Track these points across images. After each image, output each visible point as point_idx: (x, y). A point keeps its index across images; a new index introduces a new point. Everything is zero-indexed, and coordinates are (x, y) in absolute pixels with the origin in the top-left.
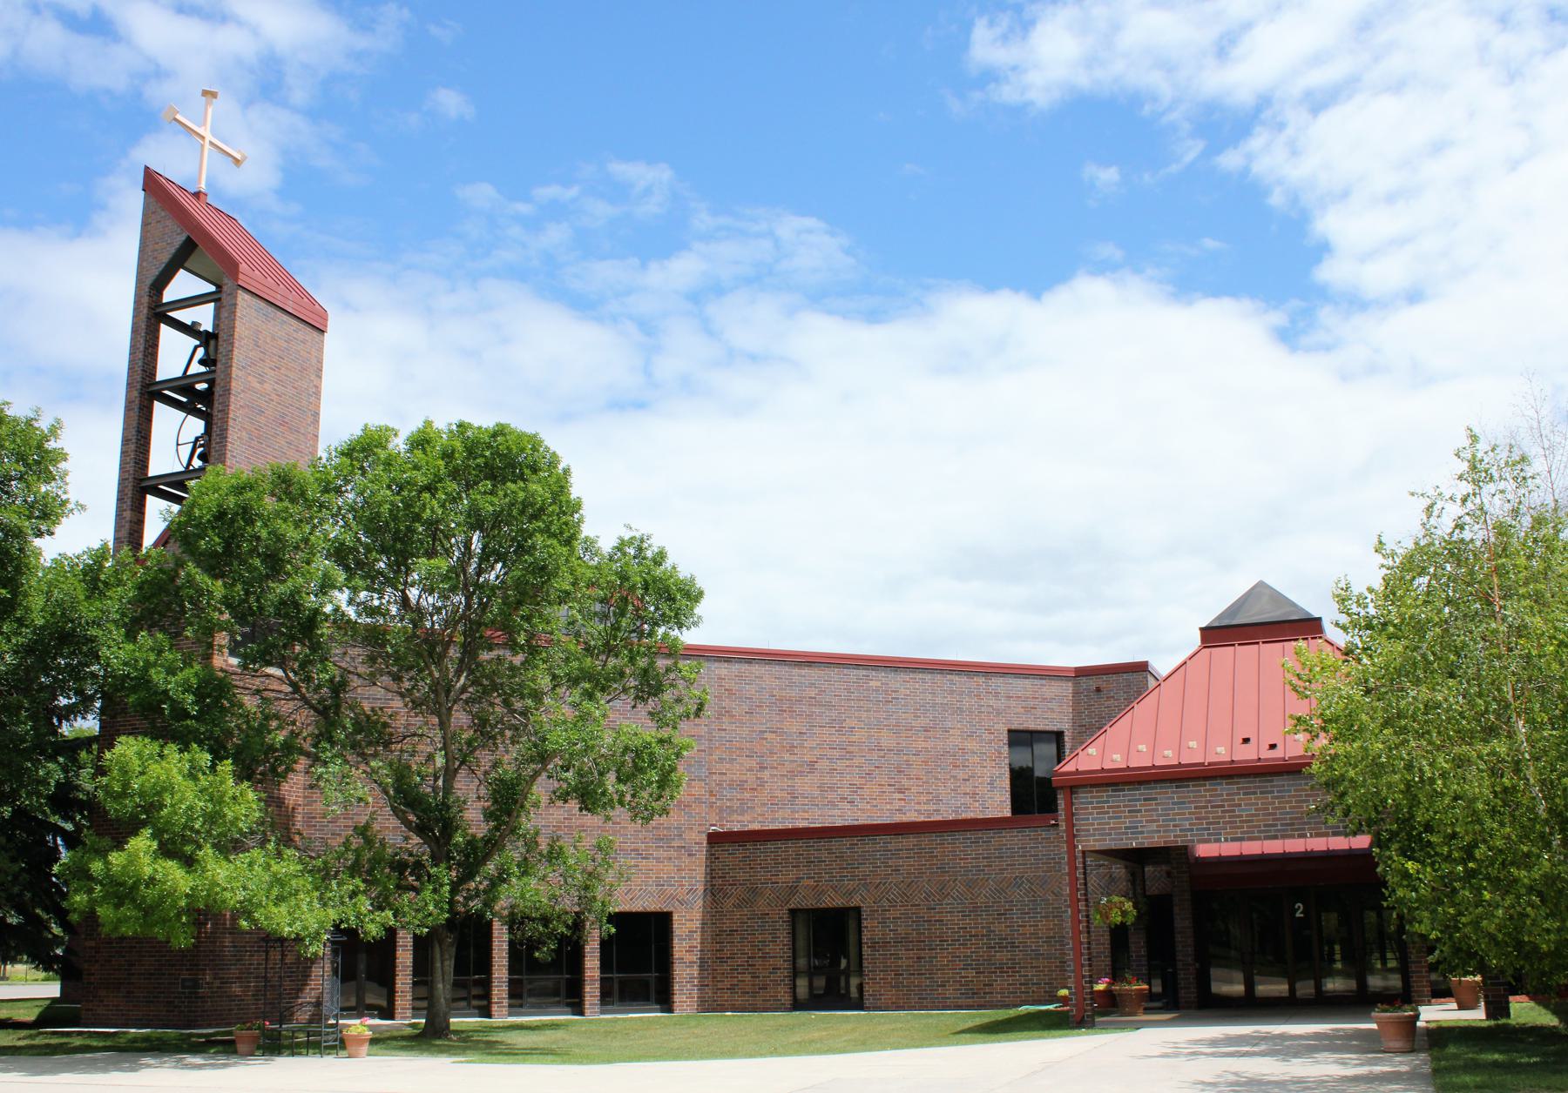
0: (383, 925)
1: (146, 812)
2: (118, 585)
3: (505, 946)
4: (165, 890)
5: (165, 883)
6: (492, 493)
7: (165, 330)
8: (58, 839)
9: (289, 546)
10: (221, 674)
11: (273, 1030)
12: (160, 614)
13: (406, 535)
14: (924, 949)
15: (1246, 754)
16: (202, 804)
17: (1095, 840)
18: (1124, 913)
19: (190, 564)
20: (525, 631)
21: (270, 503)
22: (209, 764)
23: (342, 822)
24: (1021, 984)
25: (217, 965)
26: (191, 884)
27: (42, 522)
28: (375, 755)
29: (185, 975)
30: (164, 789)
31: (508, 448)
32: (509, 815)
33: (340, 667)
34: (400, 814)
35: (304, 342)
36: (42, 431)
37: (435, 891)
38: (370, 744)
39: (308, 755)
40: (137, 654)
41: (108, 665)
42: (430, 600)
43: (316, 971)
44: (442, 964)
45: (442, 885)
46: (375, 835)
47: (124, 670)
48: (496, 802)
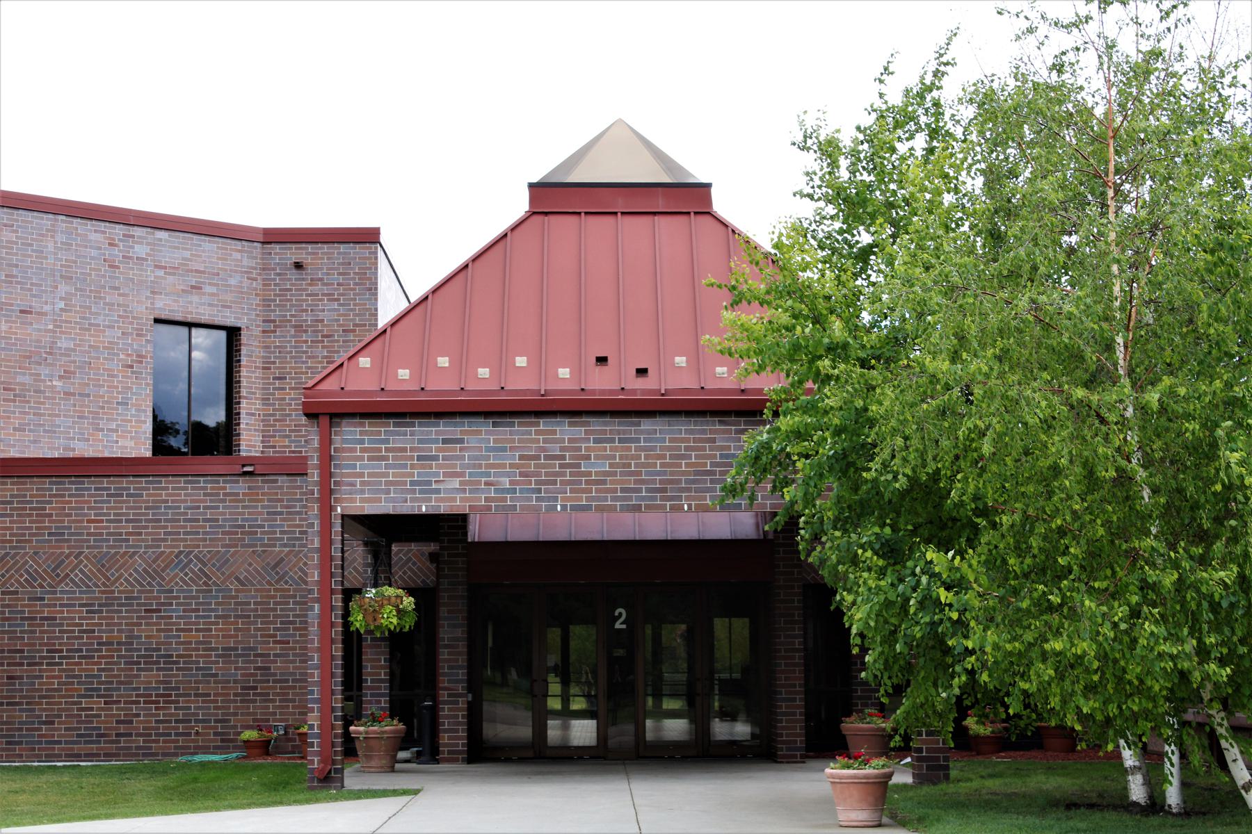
14: (22, 664)
15: (602, 383)
17: (362, 500)
18: (401, 613)
24: (177, 721)
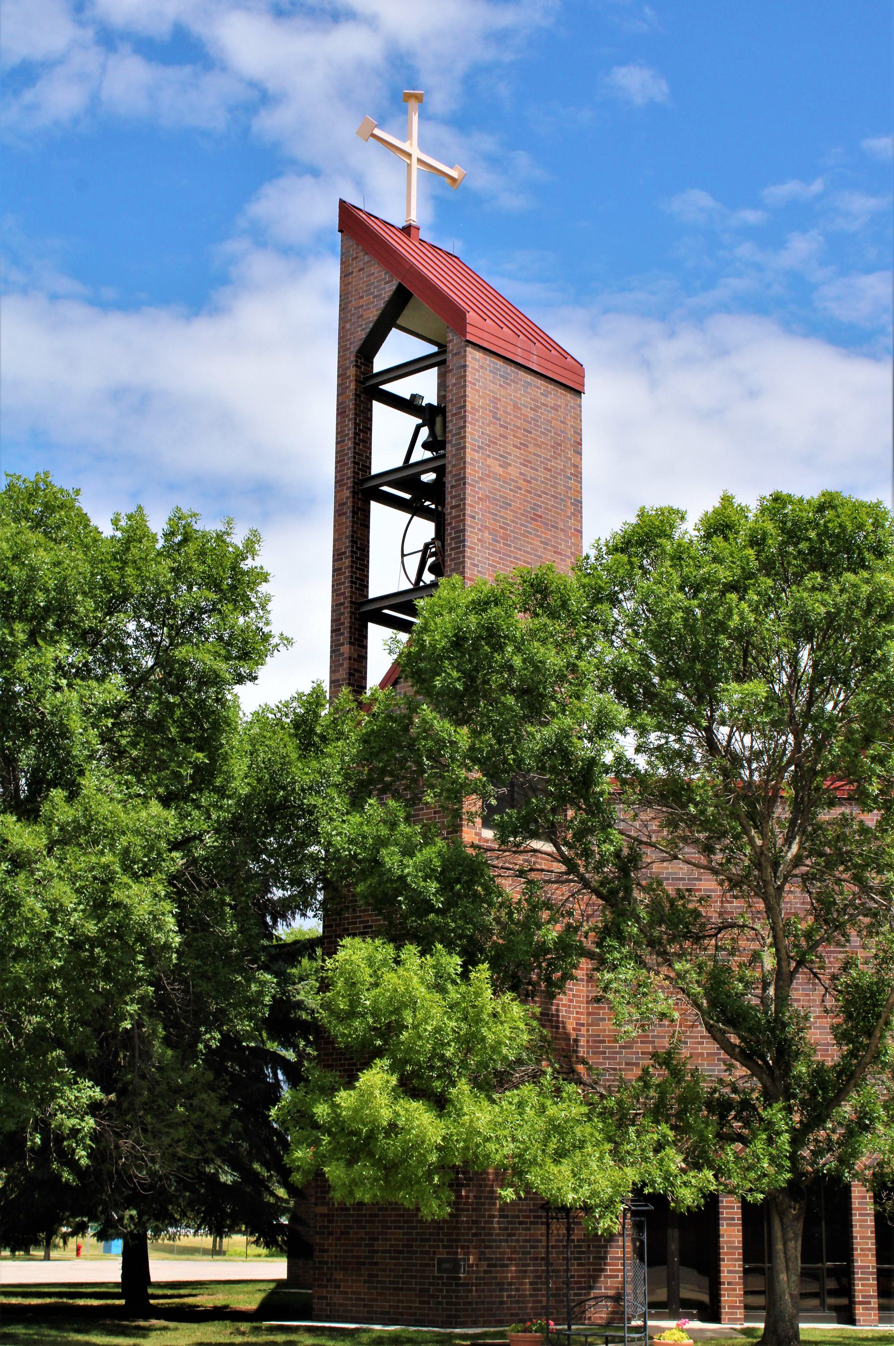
0: (700, 1190)
1: (382, 1036)
2: (338, 739)
3: (870, 1222)
4: (410, 1140)
5: (408, 1132)
6: (822, 589)
7: (378, 408)
8: (279, 1072)
9: (550, 676)
10: (470, 851)
11: (559, 1332)
12: (391, 774)
13: (706, 652)
16: (453, 1024)
19: (425, 707)
20: (879, 777)
21: (522, 622)
22: (460, 970)
23: (639, 1047)
25: (484, 1241)
26: (443, 1132)
27: (242, 663)
28: (680, 956)
29: (442, 1253)
30: (404, 1005)
31: (840, 526)
32: (869, 1034)
33: (629, 836)
34: (718, 1035)
35: (555, 408)
36: (236, 548)
37: (770, 1141)
38: (672, 940)
39: (590, 955)
40: (365, 828)
41: (330, 843)
42: (747, 739)
43: (615, 1252)
44: (785, 1245)
45: (779, 1134)
46: (684, 1064)
47: (350, 850)
48: (849, 1017)
